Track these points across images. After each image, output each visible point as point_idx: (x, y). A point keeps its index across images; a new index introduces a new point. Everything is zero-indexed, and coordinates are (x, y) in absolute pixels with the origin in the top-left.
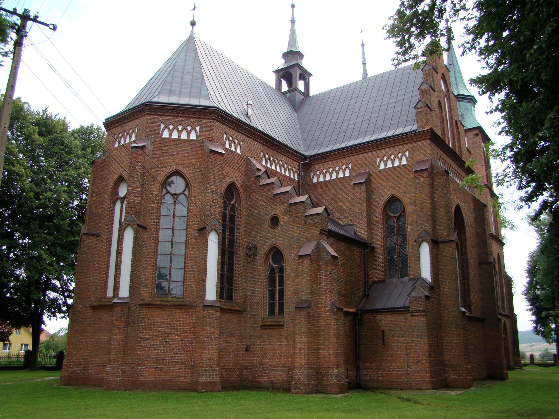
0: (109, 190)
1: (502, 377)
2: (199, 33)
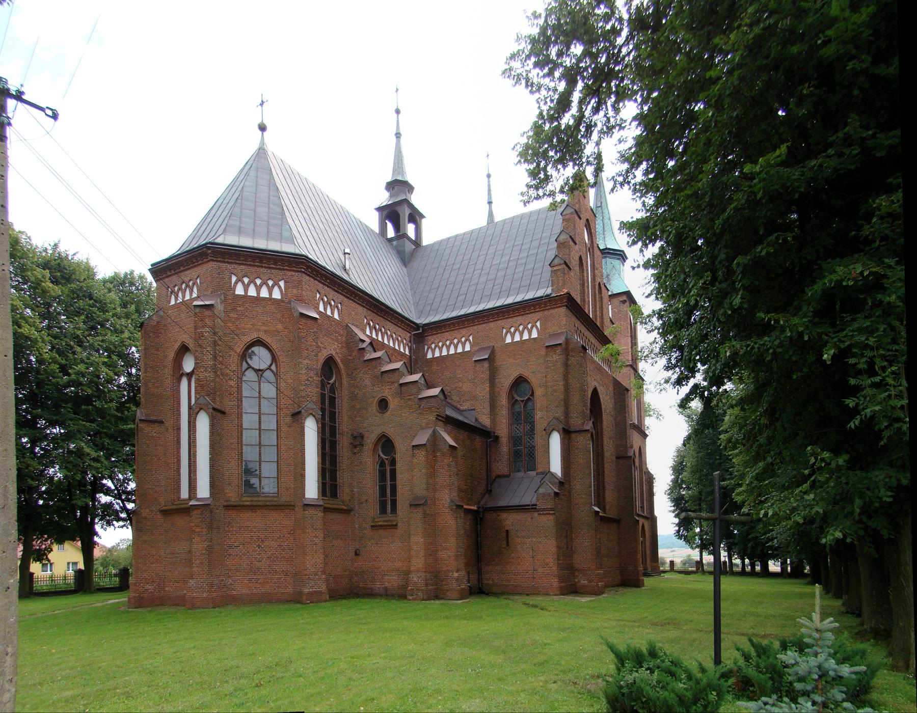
0: (169, 364)
1: (638, 584)
2: (272, 142)
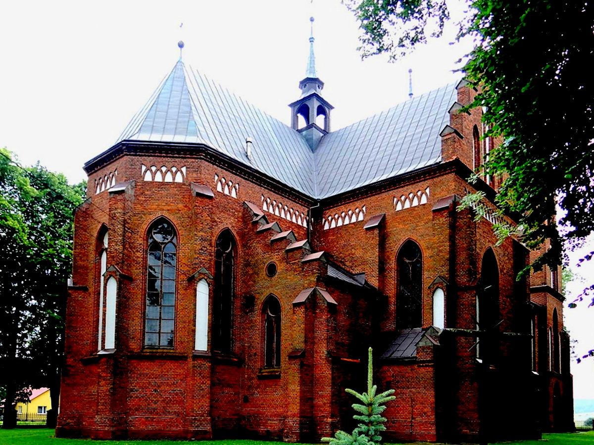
0: (93, 241)
